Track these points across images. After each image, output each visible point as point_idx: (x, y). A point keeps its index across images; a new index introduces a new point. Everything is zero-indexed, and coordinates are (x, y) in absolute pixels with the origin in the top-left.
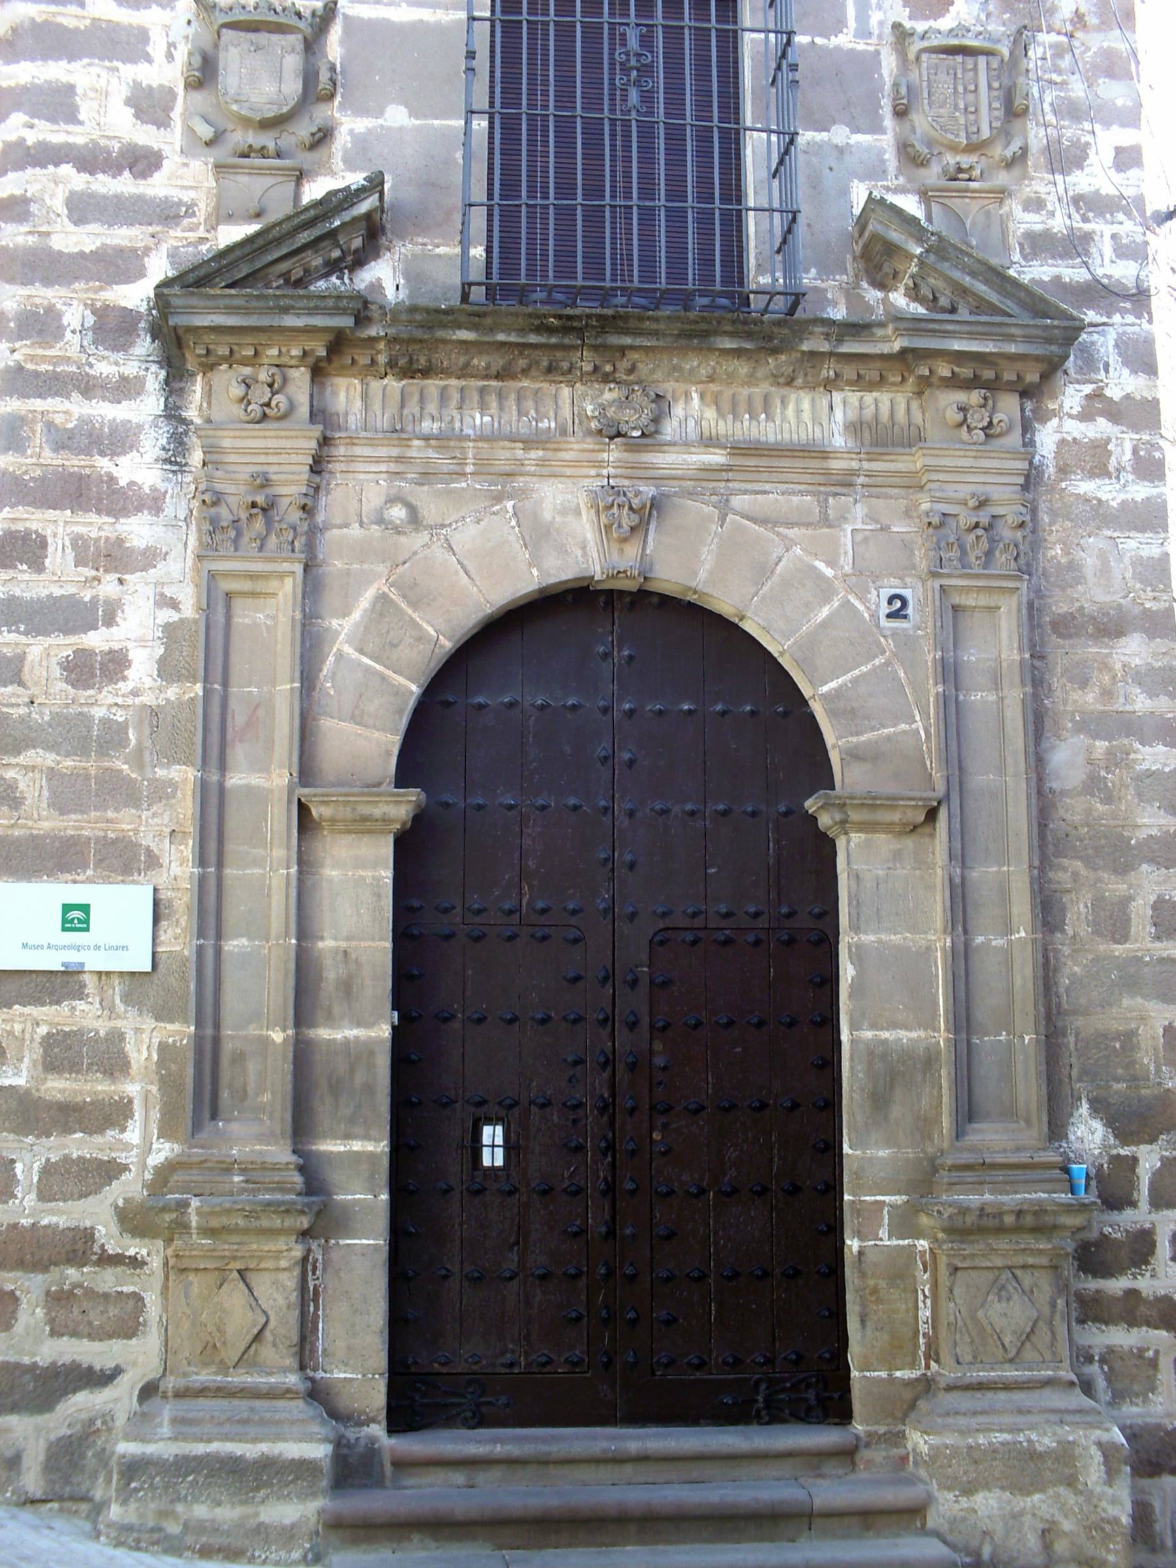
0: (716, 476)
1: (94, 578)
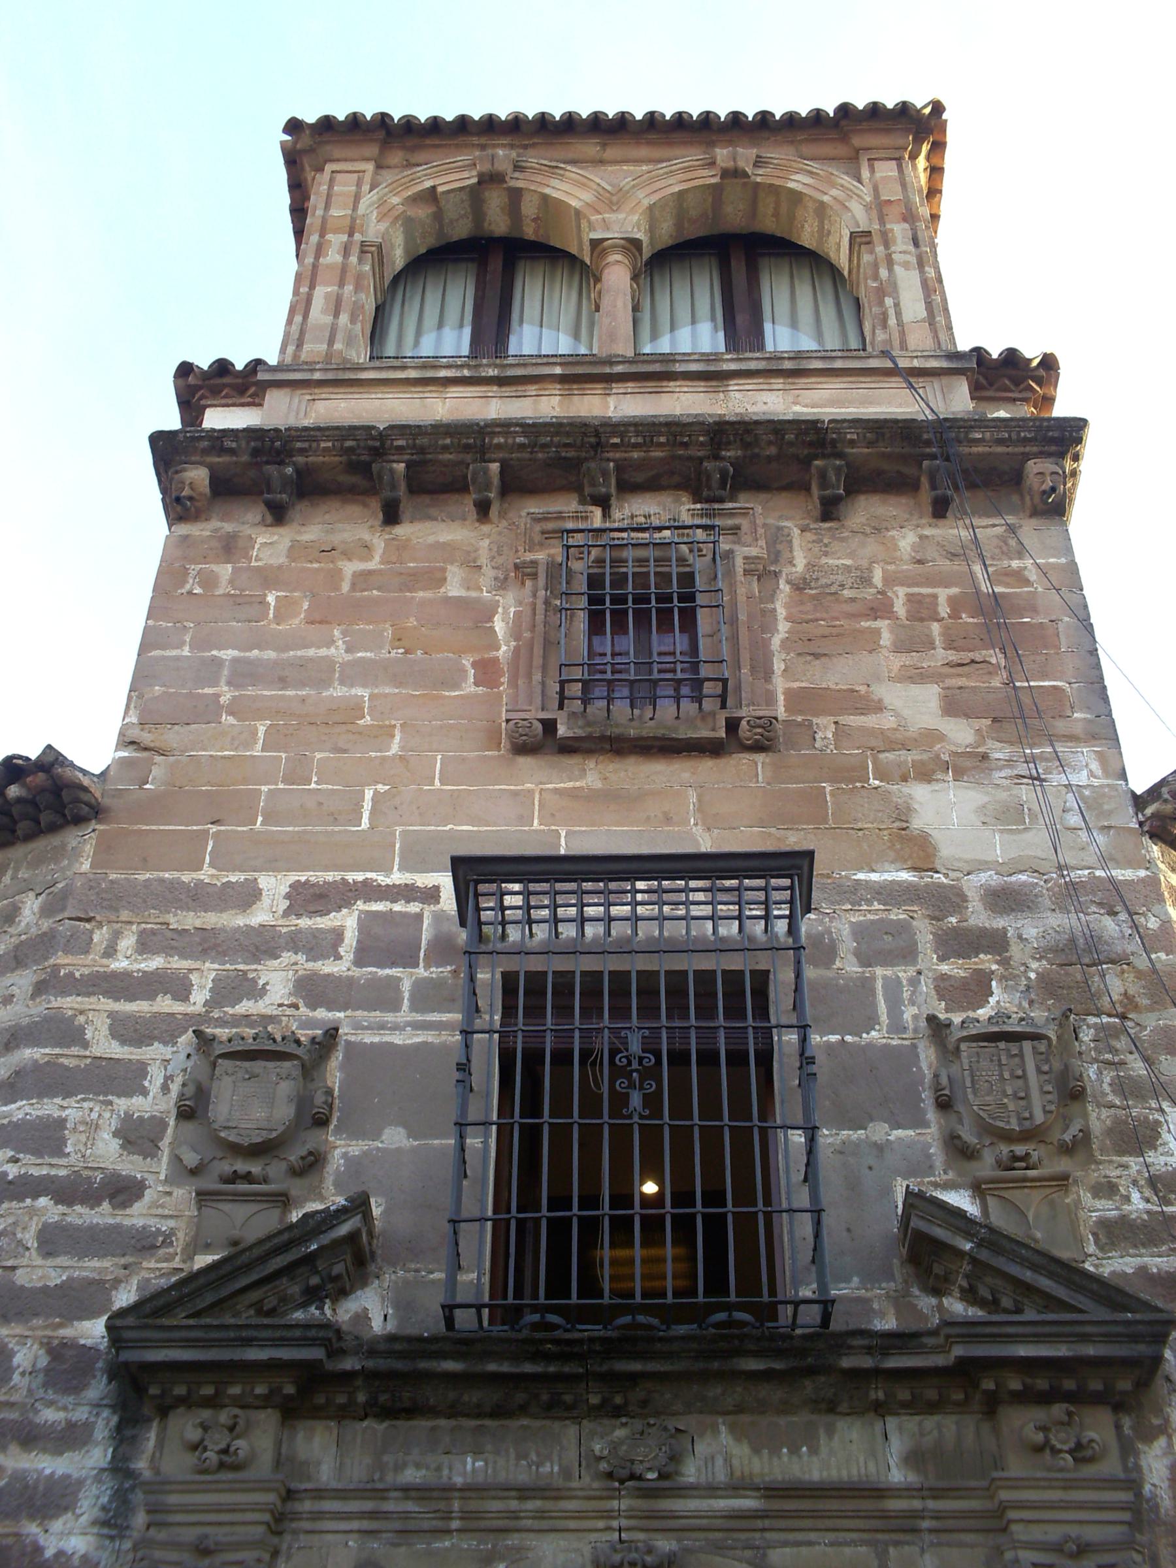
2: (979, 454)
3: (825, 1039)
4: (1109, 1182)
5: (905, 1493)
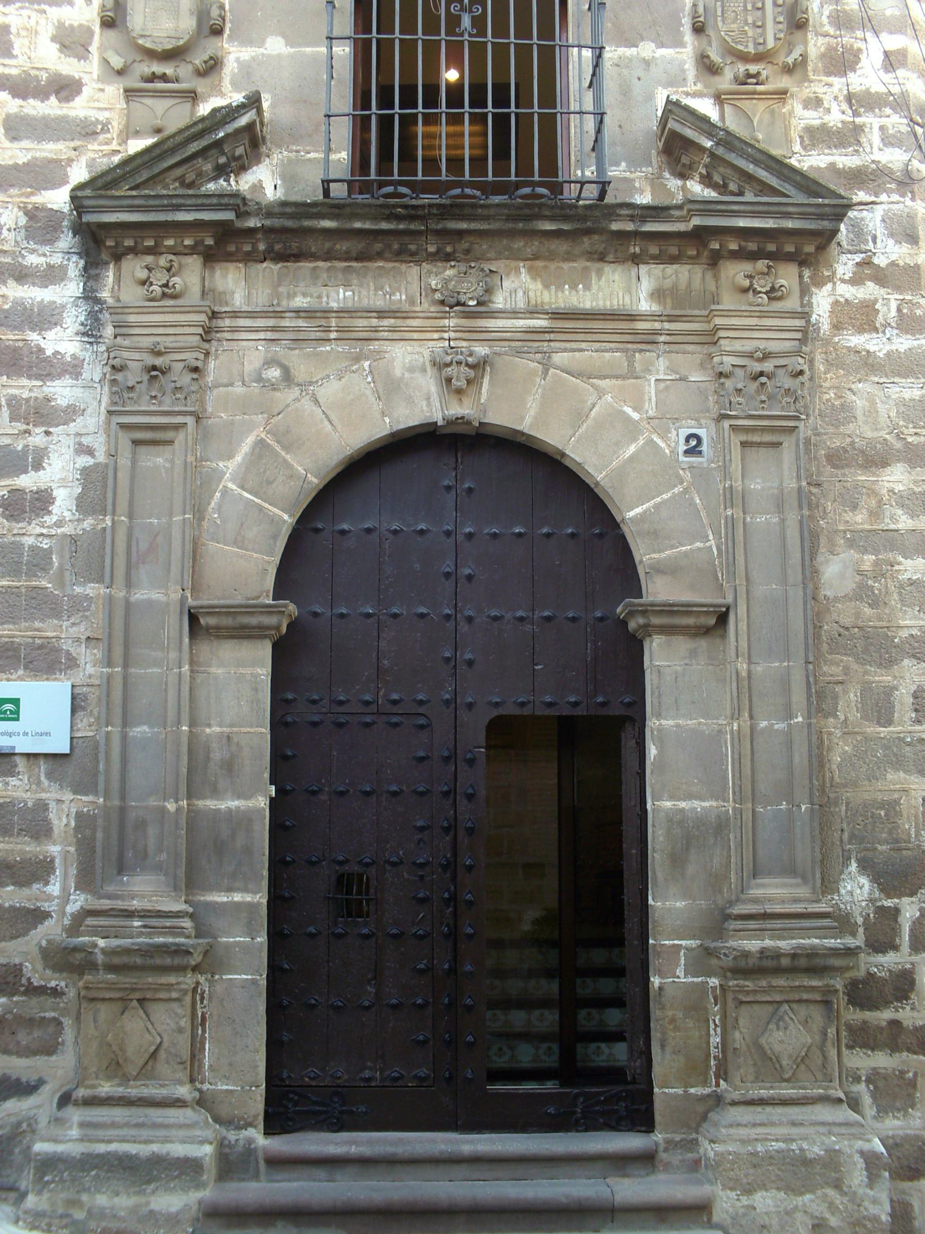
1: (26, 432)
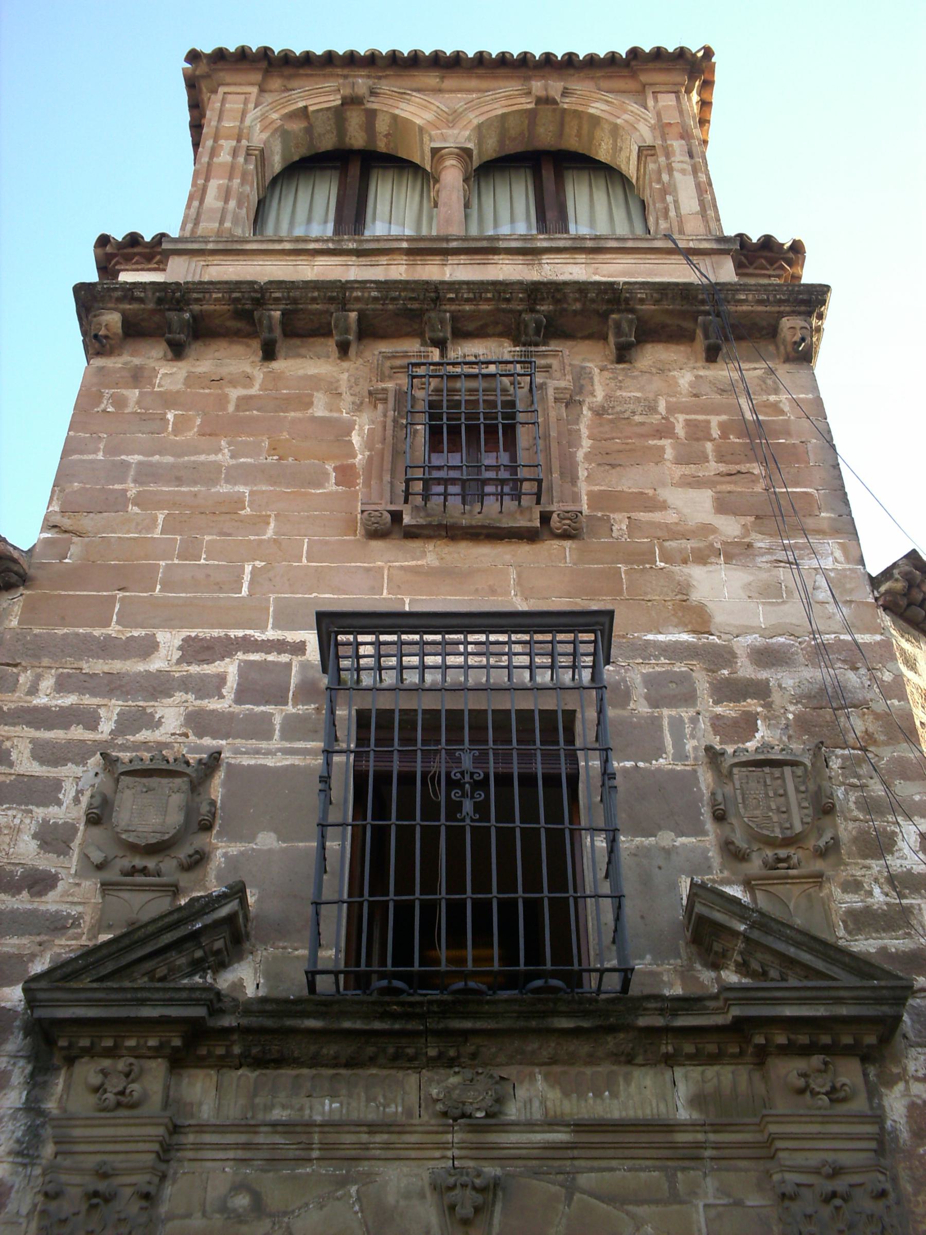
0: (560, 1154)
2: (744, 312)
3: (621, 764)
4: (855, 880)
5: (690, 1128)
